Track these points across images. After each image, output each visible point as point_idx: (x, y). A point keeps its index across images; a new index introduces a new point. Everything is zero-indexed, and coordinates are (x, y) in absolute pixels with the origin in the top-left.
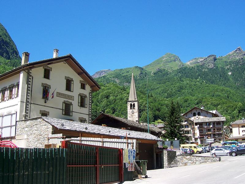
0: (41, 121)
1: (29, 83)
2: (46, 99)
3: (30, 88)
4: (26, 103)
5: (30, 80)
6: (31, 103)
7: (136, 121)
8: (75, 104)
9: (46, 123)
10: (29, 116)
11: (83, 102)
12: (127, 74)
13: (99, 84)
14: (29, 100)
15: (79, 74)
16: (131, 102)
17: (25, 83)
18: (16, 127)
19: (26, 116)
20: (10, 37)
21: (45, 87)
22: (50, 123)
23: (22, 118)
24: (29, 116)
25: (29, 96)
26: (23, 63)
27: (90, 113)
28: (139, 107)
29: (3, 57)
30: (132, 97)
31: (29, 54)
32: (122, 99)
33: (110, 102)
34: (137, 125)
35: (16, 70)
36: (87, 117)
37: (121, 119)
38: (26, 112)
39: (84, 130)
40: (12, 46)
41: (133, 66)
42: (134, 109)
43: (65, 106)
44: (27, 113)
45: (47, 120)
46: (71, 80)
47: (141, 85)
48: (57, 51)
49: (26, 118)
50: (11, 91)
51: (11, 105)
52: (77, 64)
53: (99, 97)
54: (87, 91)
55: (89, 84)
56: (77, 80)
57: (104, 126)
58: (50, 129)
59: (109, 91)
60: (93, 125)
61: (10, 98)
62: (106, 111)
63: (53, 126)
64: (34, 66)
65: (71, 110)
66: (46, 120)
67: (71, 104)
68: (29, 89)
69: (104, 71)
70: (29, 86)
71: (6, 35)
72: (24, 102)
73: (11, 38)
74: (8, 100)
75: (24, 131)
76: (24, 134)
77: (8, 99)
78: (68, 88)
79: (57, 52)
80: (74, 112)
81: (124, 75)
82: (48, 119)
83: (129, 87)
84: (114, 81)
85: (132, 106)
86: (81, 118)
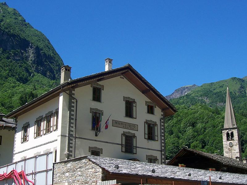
0: (86, 162)
1: (72, 108)
2: (97, 130)
3: (73, 115)
4: (68, 137)
5: (72, 104)
6: (76, 138)
7: (236, 158)
8: (140, 135)
9: (93, 165)
10: (73, 156)
11: (151, 133)
12: (221, 89)
13: (176, 106)
14: (73, 133)
15: (144, 92)
16: (228, 130)
17: (67, 109)
18: (53, 172)
19: (69, 156)
20: (54, 50)
21: (96, 113)
22: (98, 165)
23: (65, 159)
24: (73, 156)
25: (72, 127)
26: (62, 81)
27: (163, 148)
28: (240, 137)
29: (46, 76)
30: (229, 122)
31: (70, 68)
32: (214, 127)
33: (197, 132)
34: (238, 164)
35: (54, 92)
36: (158, 155)
37: (214, 156)
38: (69, 150)
39: (150, 174)
40: (57, 61)
41: (227, 77)
42: (232, 140)
43: (126, 140)
44: (71, 152)
45: (94, 161)
46: (133, 101)
47: (242, 105)
48: (110, 61)
49: (70, 157)
50: (49, 122)
51: (49, 141)
52: (140, 78)
53: (182, 125)
54: (157, 116)
55: (160, 107)
56: (141, 102)
57: (182, 166)
58: (100, 174)
59: (196, 115)
60: (164, 166)
61: (48, 131)
62: (192, 145)
63: (103, 169)
64: (77, 84)
65: (134, 145)
66: (93, 160)
67: (134, 136)
68: (72, 117)
69: (187, 88)
70: (72, 113)
71: (49, 47)
72: (66, 136)
73: (55, 51)
74: (45, 134)
75: (64, 177)
76: (64, 182)
77: (45, 133)
78: (129, 113)
79: (110, 62)
80: (138, 147)
81: (215, 91)
82: (96, 159)
83: (223, 109)
84: (202, 102)
85: (230, 136)
86: (149, 156)
